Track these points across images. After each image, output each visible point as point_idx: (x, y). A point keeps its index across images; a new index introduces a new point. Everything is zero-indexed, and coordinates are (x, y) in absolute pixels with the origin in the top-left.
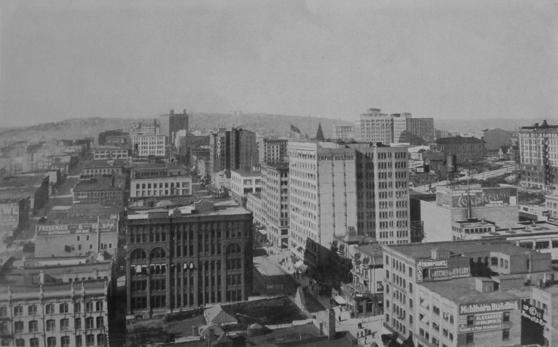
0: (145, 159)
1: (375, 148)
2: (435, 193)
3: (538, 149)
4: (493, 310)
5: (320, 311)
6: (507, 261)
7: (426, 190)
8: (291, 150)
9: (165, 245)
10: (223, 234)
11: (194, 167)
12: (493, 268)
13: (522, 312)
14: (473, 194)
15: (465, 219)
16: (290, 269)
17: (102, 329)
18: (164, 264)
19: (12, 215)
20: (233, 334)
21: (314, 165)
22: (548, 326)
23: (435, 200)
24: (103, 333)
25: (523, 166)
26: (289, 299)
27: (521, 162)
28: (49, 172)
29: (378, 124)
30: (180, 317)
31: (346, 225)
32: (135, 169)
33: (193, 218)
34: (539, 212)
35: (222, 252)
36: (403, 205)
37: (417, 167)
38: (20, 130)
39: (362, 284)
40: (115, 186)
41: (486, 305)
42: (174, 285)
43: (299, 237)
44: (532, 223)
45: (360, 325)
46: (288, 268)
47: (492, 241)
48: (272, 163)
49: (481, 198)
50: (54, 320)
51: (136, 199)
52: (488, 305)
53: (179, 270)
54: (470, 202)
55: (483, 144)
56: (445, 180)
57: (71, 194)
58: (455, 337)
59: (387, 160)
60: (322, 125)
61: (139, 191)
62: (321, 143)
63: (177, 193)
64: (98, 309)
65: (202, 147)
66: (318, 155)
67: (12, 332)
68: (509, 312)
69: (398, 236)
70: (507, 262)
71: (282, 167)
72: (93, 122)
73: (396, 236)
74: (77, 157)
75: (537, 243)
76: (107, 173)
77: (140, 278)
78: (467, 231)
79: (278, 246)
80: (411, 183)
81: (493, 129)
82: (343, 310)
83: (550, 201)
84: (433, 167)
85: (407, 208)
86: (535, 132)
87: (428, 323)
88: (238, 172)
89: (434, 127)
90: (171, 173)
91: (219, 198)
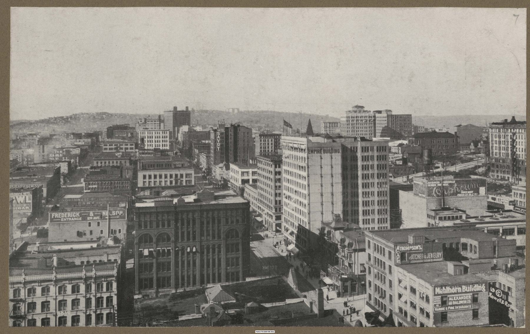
0: (151, 152)
1: (359, 142)
2: (413, 183)
3: (506, 143)
4: (463, 291)
5: (310, 290)
6: (475, 247)
7: (404, 180)
8: (284, 144)
9: (171, 232)
10: (223, 221)
11: (196, 160)
12: (463, 253)
13: (489, 295)
14: (447, 185)
15: (439, 208)
16: (283, 251)
17: (111, 308)
18: (170, 248)
19: (26, 203)
20: (232, 312)
21: (305, 159)
22: (513, 307)
23: (412, 190)
24: (112, 311)
25: (492, 159)
26: (282, 279)
27: (491, 155)
28: (60, 163)
29: (362, 120)
30: (183, 296)
31: (333, 213)
32: (141, 161)
33: (196, 206)
34: (506, 201)
35: (222, 237)
36: (383, 195)
37: (396, 160)
38: (30, 123)
39: (347, 266)
40: (124, 177)
41: (457, 287)
42: (178, 267)
43: (291, 222)
44: (499, 212)
45: (345, 304)
46: (281, 250)
47: (463, 228)
48: (267, 155)
49: (453, 188)
50: (66, 300)
51: (143, 189)
52: (459, 287)
53: (183, 254)
54: (444, 192)
55: (457, 140)
56: (421, 172)
57: (82, 183)
58: (432, 315)
59: (370, 153)
60: (311, 120)
61: (151, 181)
62: (311, 138)
63: (181, 183)
64: (108, 289)
65: (204, 141)
66: (308, 149)
67: (25, 312)
68: (478, 294)
69: (378, 222)
70: (476, 247)
71: (276, 158)
72: (102, 116)
73: (377, 223)
74: (86, 150)
75: (503, 230)
76: (115, 164)
77: (148, 261)
78: (440, 219)
79: (272, 231)
80: (391, 175)
81: (465, 124)
82: (331, 290)
83: (516, 192)
84: (410, 160)
85: (387, 197)
86: (504, 128)
87: (406, 302)
88: (236, 165)
89: (412, 123)
90: (175, 165)
91: (219, 188)
